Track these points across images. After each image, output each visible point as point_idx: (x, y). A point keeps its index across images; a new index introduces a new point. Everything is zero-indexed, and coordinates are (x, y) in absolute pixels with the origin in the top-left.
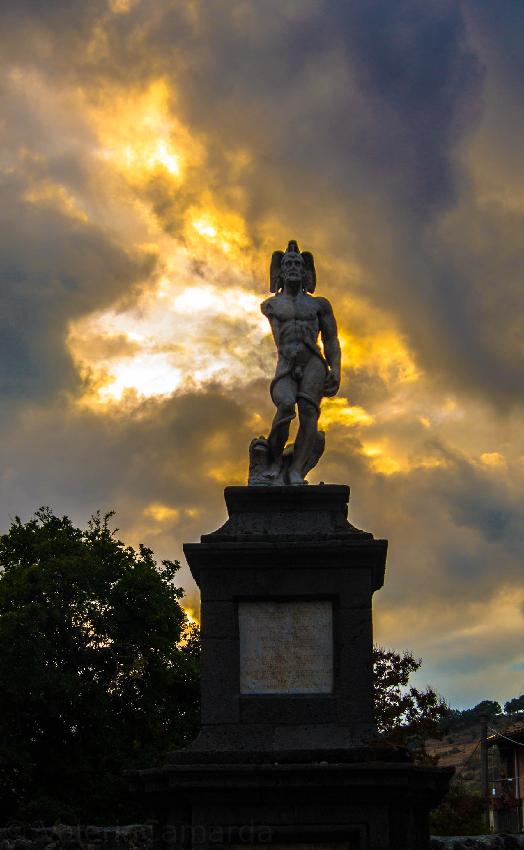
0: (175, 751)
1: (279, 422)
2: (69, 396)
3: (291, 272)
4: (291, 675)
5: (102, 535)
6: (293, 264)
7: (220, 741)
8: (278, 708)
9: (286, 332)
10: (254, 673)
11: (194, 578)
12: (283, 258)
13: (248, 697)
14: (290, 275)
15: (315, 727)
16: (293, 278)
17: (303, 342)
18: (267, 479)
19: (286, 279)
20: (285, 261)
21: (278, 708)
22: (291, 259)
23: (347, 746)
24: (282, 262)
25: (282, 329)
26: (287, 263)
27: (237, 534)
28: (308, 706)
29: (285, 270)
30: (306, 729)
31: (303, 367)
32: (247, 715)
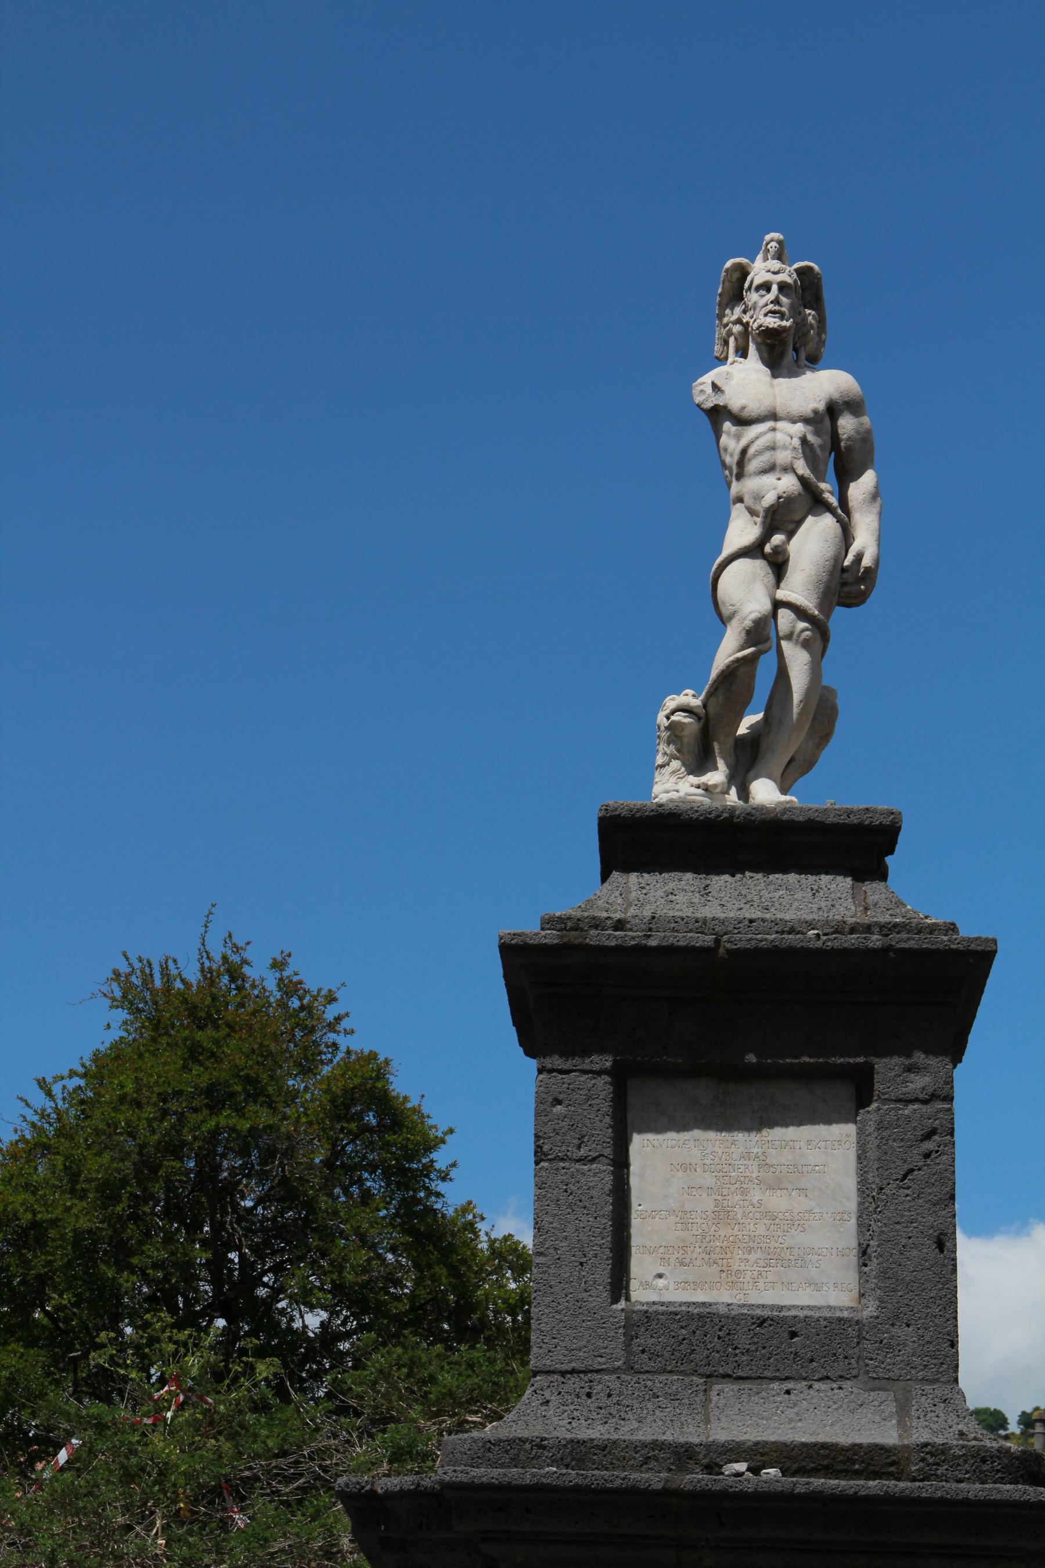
0: (466, 1435)
1: (732, 658)
2: (409, 1105)
3: (771, 307)
4: (752, 1257)
5: (424, 1165)
6: (775, 288)
7: (576, 1414)
8: (719, 1338)
9: (751, 451)
10: (662, 1250)
11: (514, 1025)
12: (749, 278)
13: (645, 1308)
14: (766, 315)
15: (810, 1387)
16: (772, 322)
17: (794, 471)
18: (700, 791)
19: (755, 326)
20: (756, 282)
21: (719, 1338)
22: (769, 277)
23: (889, 1436)
24: (746, 285)
25: (744, 442)
26: (759, 288)
27: (629, 914)
28: (793, 1335)
29: (755, 303)
30: (788, 1392)
31: (791, 534)
32: (643, 1351)
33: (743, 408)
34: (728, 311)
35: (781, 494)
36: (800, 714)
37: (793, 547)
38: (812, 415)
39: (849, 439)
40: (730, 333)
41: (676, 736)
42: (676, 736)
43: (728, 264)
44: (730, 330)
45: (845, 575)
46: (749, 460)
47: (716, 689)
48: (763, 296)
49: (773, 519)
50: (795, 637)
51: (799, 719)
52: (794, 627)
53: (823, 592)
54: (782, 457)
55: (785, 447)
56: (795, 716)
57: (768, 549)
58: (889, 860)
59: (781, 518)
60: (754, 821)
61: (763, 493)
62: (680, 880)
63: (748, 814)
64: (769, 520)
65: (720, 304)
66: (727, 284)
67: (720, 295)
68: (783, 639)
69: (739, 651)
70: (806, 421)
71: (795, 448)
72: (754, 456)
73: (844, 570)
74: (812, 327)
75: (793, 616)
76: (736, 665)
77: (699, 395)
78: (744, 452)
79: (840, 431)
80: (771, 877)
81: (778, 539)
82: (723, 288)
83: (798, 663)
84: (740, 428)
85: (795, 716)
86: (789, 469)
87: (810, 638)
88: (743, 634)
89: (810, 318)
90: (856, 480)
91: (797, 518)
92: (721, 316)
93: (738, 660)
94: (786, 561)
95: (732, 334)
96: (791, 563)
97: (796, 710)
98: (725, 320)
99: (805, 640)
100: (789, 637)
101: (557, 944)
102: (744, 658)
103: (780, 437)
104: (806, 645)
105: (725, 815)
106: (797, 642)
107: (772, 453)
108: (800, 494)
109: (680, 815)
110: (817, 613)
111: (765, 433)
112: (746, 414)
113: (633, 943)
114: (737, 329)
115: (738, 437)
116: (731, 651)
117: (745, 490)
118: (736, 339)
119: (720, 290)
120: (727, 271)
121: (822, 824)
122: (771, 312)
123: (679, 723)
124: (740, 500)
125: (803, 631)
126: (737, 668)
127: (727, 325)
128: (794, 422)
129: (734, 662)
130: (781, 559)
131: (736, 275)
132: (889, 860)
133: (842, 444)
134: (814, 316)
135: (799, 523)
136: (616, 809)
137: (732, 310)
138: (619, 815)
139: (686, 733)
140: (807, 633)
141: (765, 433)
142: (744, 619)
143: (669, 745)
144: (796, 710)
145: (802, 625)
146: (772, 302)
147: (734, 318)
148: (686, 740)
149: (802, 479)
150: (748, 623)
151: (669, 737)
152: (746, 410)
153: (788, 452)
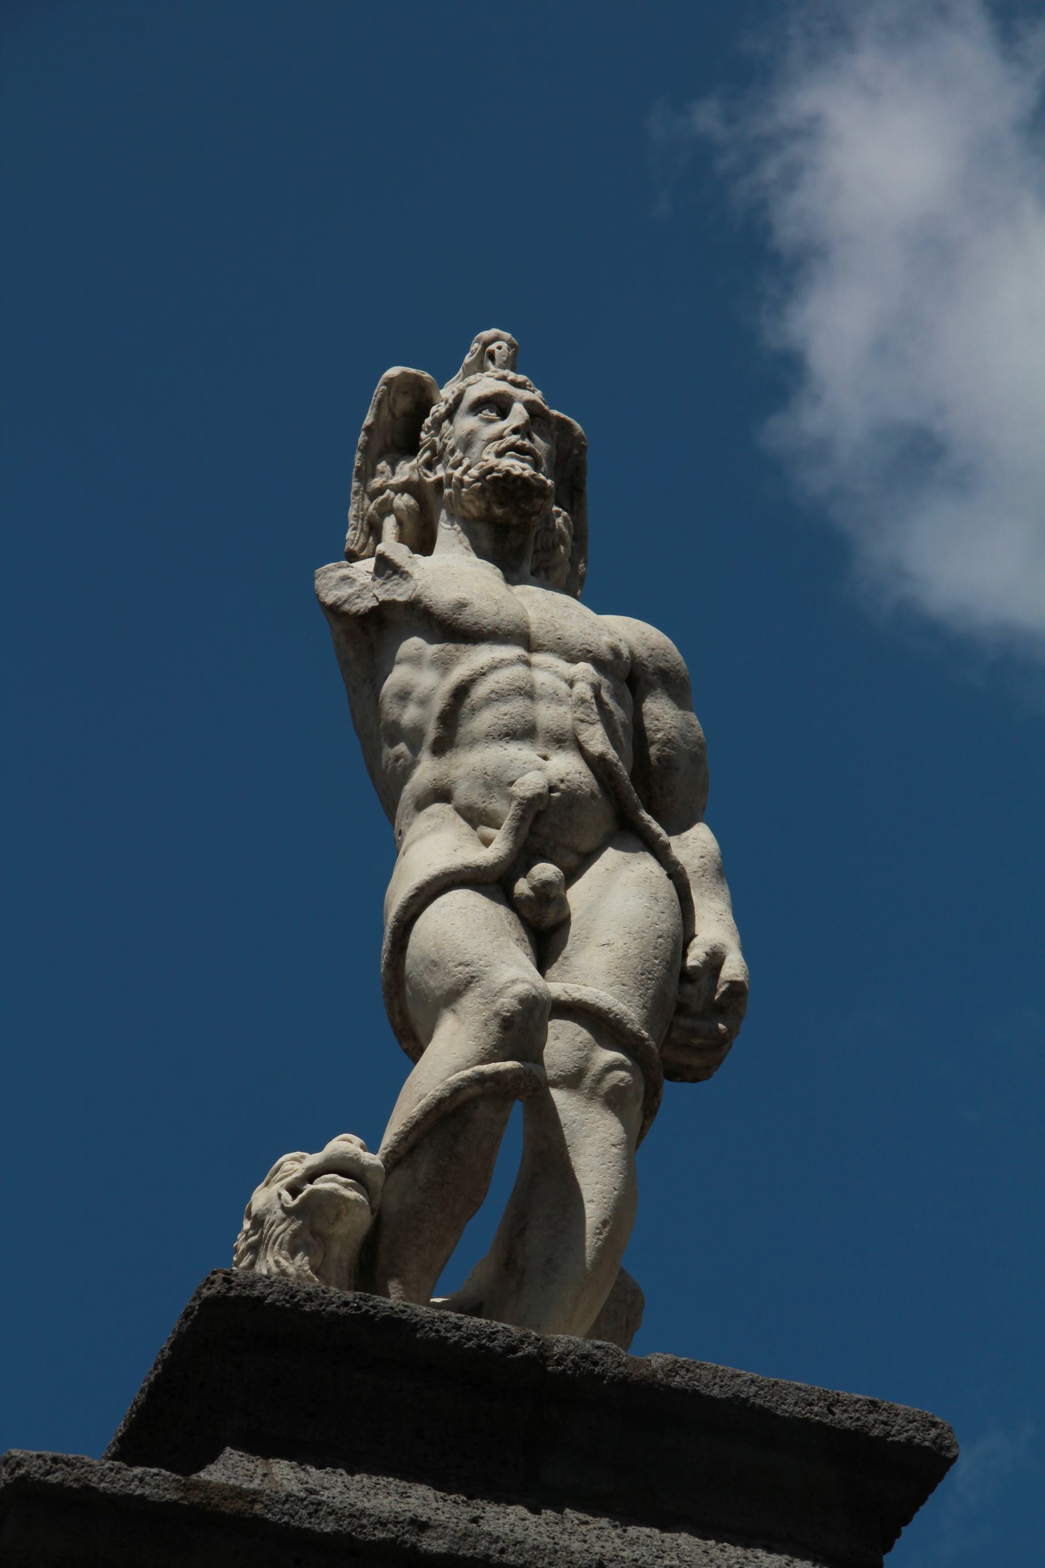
1: (468, 1072)
9: (480, 691)
25: (459, 673)
31: (572, 875)
33: (462, 605)
34: (382, 465)
35: (555, 781)
36: (601, 1251)
37: (577, 895)
38: (610, 657)
39: (668, 742)
40: (387, 509)
41: (314, 1233)
42: (314, 1233)
43: (394, 371)
44: (388, 502)
45: (689, 988)
46: (474, 710)
47: (412, 1150)
48: (491, 421)
49: (532, 832)
50: (588, 1081)
51: (597, 1263)
52: (587, 1059)
53: (653, 997)
54: (549, 715)
55: (556, 698)
56: (589, 1254)
57: (522, 887)
58: (903, 1529)
59: (553, 833)
60: (601, 1377)
61: (510, 775)
62: (404, 1495)
63: (585, 1357)
64: (525, 830)
65: (366, 449)
66: (385, 412)
67: (369, 430)
68: (555, 1084)
69: (483, 1062)
70: (598, 663)
71: (583, 701)
72: (489, 701)
73: (686, 976)
74: (562, 540)
75: (585, 1035)
76: (476, 1090)
77: (336, 586)
78: (461, 692)
79: (647, 723)
80: (633, 1531)
81: (545, 871)
82: (377, 416)
83: (594, 1145)
84: (450, 647)
85: (589, 1254)
86: (565, 740)
87: (628, 1086)
88: (494, 1026)
89: (559, 521)
90: (559, 954)
91: (585, 846)
92: (367, 473)
93: (481, 1079)
94: (564, 923)
95: (391, 511)
96: (573, 930)
97: (591, 1241)
98: (377, 482)
99: (615, 1089)
100: (572, 1081)
101: (173, 1504)
102: (497, 1076)
103: (542, 678)
104: (614, 1101)
105: (528, 1349)
106: (592, 1095)
107: (528, 702)
108: (593, 795)
109: (415, 1327)
110: (646, 1034)
111: (511, 663)
112: (466, 617)
113: (380, 1535)
114: (403, 501)
115: (444, 665)
116: (460, 1061)
117: (455, 773)
118: (400, 523)
119: (368, 420)
120: (390, 382)
121: (765, 1415)
122: (512, 447)
123: (331, 1195)
124: (442, 794)
125: (611, 1067)
126: (473, 1100)
127: (381, 491)
128: (573, 660)
129: (471, 1081)
130: (551, 916)
131: (403, 403)
132: (903, 1529)
133: (653, 750)
134: (565, 518)
135: (589, 858)
136: (252, 1285)
137: (393, 465)
138: (261, 1299)
139: (341, 1229)
140: (622, 1074)
141: (511, 663)
142: (499, 993)
143: (293, 1254)
144: (591, 1241)
145: (607, 1056)
146: (515, 431)
147: (399, 478)
148: (336, 1249)
149: (596, 764)
150: (507, 1002)
151: (295, 1235)
152: (468, 611)
153: (563, 709)
